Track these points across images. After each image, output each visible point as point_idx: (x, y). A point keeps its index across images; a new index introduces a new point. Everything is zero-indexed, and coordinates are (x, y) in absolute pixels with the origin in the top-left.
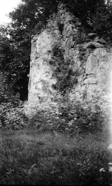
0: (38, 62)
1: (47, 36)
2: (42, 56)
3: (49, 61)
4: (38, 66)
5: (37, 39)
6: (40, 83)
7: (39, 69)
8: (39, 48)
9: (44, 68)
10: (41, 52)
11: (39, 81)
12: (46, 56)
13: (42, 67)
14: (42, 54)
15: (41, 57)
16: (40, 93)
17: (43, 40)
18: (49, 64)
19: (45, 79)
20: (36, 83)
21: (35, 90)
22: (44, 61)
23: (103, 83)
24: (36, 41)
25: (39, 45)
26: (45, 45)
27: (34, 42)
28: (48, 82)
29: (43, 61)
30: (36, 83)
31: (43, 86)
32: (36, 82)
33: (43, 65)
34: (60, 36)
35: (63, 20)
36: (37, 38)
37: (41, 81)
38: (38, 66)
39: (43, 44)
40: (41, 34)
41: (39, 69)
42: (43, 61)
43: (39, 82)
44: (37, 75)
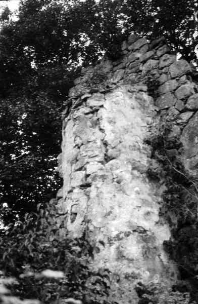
0: (118, 172)
1: (129, 101)
2: (126, 153)
3: (145, 169)
4: (119, 182)
5: (102, 106)
6: (131, 236)
7: (122, 190)
8: (113, 132)
9: (137, 189)
10: (120, 142)
11: (126, 229)
12: (135, 155)
13: (131, 185)
14: (125, 148)
15: (123, 157)
16: (137, 272)
17: (120, 111)
18: (147, 180)
19: (146, 225)
20: (118, 236)
21: (115, 263)
22: (134, 169)
23: (140, 296)
24: (97, 110)
25: (110, 122)
26: (128, 125)
27: (91, 115)
28: (153, 234)
29: (130, 169)
30: (118, 238)
31: (143, 247)
32: (114, 234)
33: (133, 181)
34: (155, 110)
35: (46, 199)
36: (101, 104)
37: (134, 231)
38: (119, 182)
39: (121, 123)
40: (111, 94)
41: (122, 190)
42: (130, 167)
43: (128, 236)
44: (117, 210)
